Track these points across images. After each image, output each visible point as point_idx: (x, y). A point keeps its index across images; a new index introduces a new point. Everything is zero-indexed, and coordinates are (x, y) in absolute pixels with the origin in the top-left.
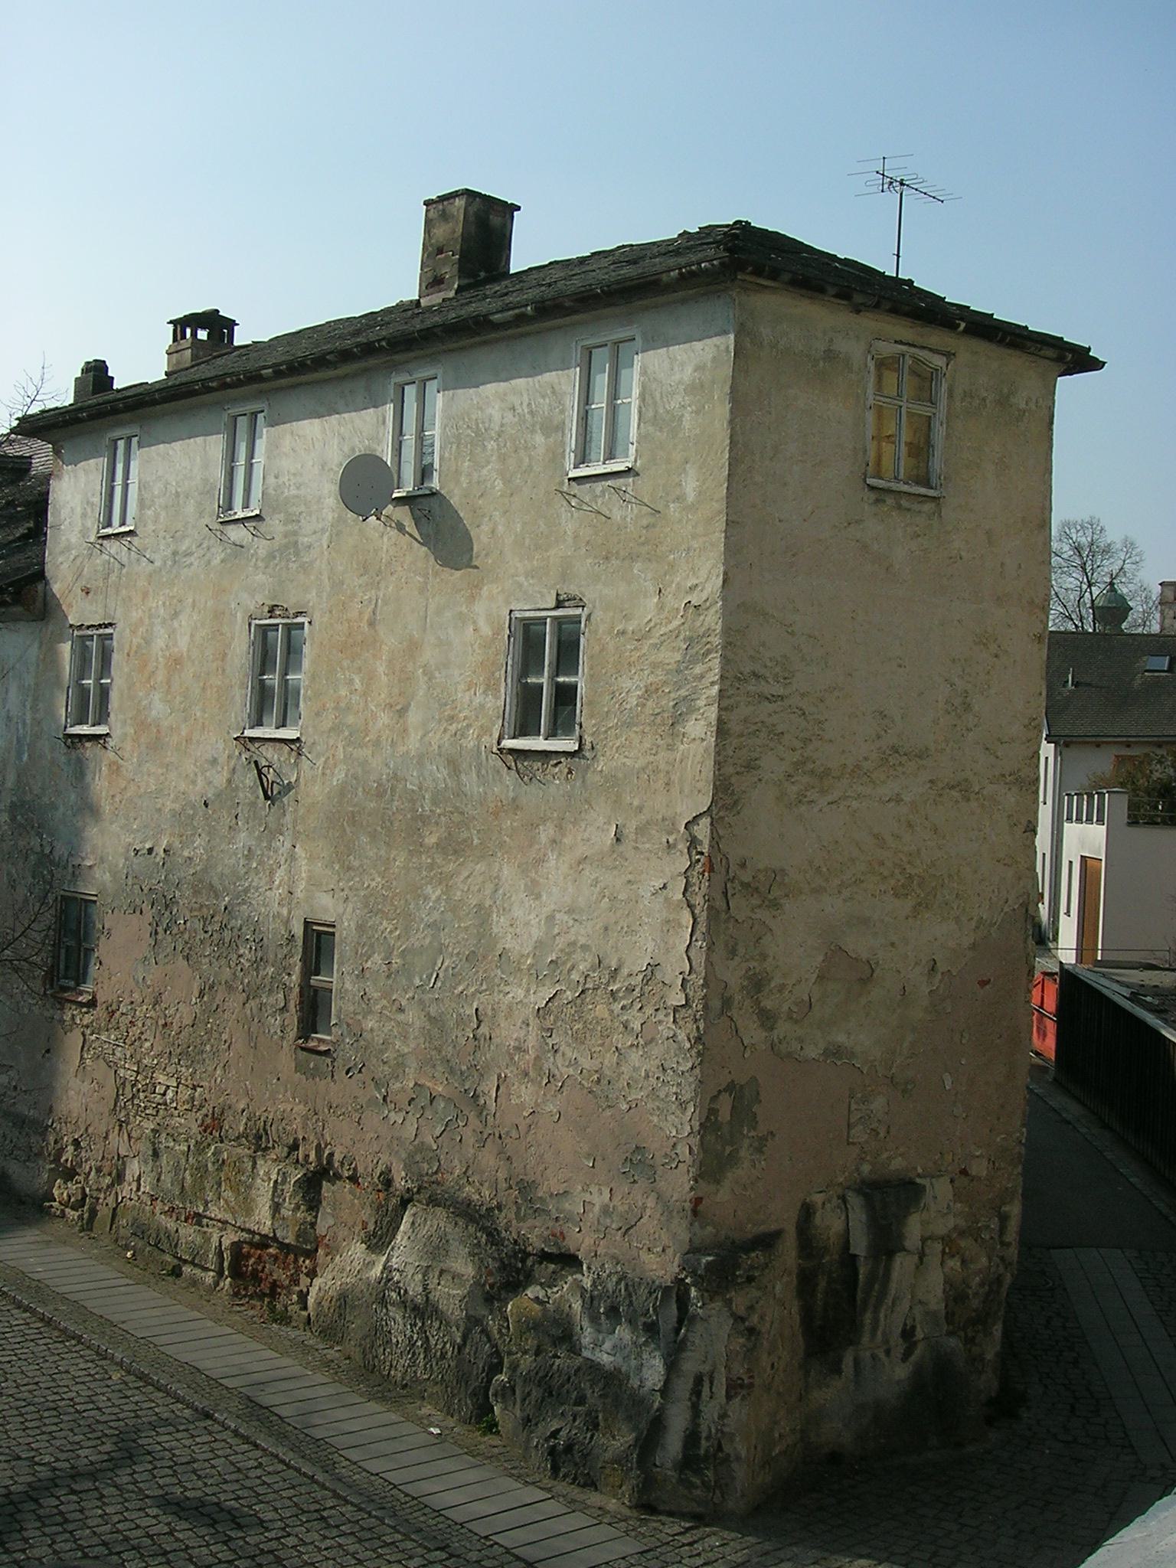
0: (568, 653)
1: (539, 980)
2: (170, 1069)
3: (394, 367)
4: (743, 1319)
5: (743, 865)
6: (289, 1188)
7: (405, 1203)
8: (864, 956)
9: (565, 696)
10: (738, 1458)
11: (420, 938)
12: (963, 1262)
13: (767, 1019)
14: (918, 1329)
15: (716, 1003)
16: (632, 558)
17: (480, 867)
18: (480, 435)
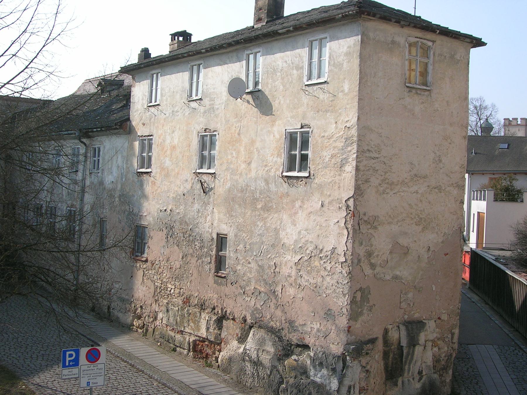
0: (305, 144)
2: (173, 283)
3: (246, 48)
4: (365, 367)
5: (365, 214)
7: (251, 327)
9: (304, 158)
11: (256, 239)
12: (439, 349)
13: (373, 266)
14: (424, 371)
15: (356, 261)
16: (327, 111)
18: (275, 71)
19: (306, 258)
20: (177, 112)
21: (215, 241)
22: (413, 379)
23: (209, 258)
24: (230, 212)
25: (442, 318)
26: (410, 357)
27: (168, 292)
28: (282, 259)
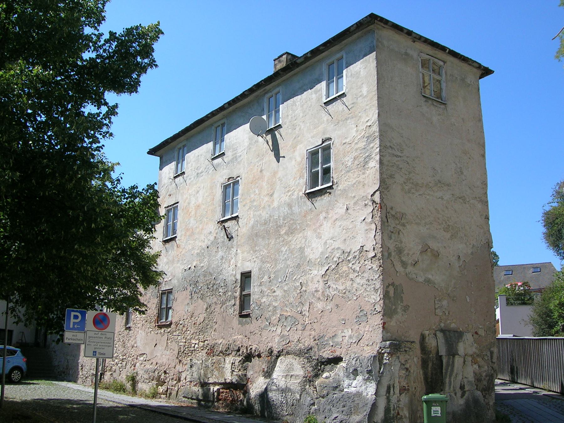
0: (327, 159)
1: (322, 265)
2: (197, 338)
4: (404, 365)
5: (392, 208)
6: (237, 364)
7: (278, 357)
8: (436, 249)
9: (327, 171)
10: (405, 417)
11: (280, 266)
12: (479, 366)
13: (404, 264)
14: (466, 386)
15: (386, 254)
16: (346, 119)
17: (301, 235)
19: (333, 266)
20: (202, 173)
21: (239, 281)
22: (456, 394)
23: (233, 301)
24: (254, 249)
25: (480, 333)
26: (450, 368)
27: (192, 349)
28: (308, 276)
